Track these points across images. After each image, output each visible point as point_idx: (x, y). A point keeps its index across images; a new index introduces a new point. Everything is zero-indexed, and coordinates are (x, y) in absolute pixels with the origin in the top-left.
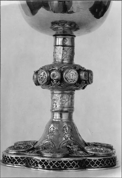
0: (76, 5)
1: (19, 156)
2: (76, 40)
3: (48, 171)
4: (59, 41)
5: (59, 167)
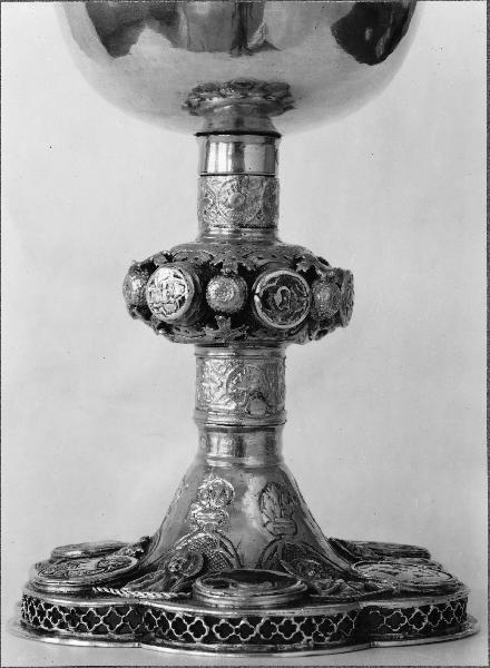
0: (275, 17)
1: (92, 605)
2: (283, 146)
3: (223, 655)
4: (221, 157)
5: (271, 638)
